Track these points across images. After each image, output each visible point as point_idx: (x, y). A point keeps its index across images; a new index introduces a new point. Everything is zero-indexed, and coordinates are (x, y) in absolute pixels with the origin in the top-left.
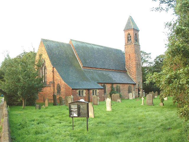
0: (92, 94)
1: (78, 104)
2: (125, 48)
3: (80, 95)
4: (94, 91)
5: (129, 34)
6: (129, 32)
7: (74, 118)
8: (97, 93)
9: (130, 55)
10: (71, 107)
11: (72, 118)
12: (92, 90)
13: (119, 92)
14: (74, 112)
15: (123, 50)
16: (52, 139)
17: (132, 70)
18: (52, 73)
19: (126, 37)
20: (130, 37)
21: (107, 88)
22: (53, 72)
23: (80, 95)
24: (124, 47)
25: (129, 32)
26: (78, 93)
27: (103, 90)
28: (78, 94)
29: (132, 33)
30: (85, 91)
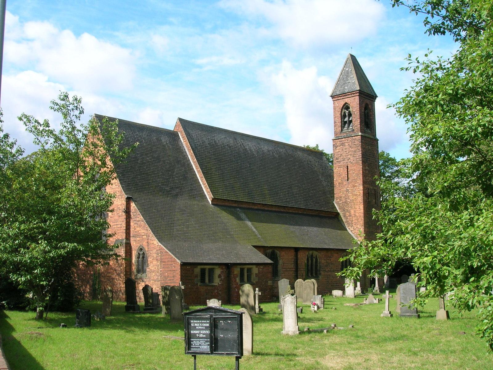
0: (238, 280)
1: (211, 316)
2: (335, 146)
3: (203, 280)
4: (245, 271)
5: (347, 108)
6: (346, 100)
7: (197, 356)
8: (253, 277)
9: (349, 168)
10: (192, 325)
11: (195, 357)
12: (239, 267)
13: (316, 274)
14: (199, 338)
15: (327, 148)
16: (372, 368)
17: (352, 211)
18: (124, 214)
19: (338, 115)
20: (350, 115)
21: (281, 262)
22: (128, 211)
23: (203, 280)
24: (332, 143)
25: (346, 100)
26: (199, 274)
27: (270, 269)
28: (199, 278)
29: (354, 103)
30: (218, 271)
